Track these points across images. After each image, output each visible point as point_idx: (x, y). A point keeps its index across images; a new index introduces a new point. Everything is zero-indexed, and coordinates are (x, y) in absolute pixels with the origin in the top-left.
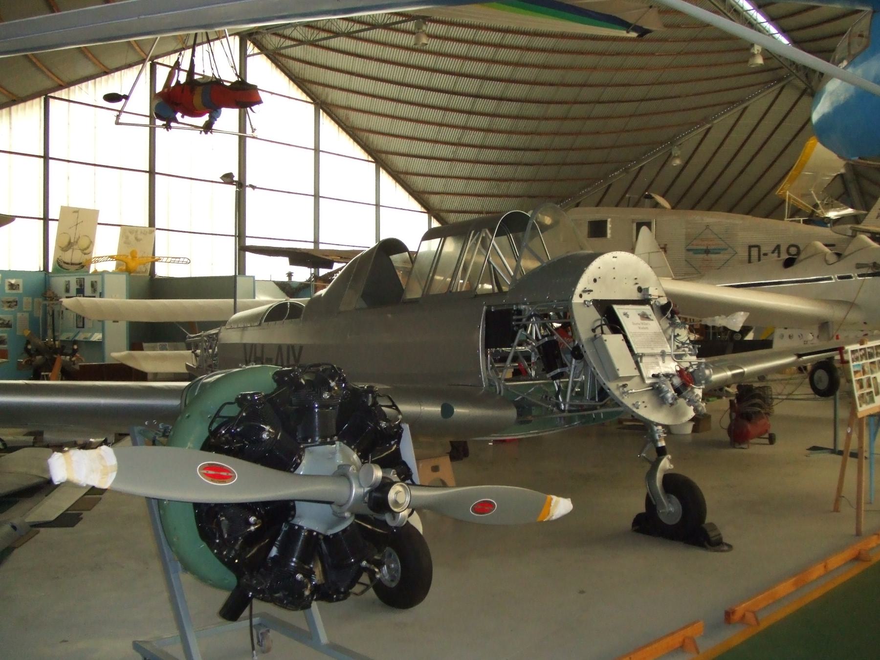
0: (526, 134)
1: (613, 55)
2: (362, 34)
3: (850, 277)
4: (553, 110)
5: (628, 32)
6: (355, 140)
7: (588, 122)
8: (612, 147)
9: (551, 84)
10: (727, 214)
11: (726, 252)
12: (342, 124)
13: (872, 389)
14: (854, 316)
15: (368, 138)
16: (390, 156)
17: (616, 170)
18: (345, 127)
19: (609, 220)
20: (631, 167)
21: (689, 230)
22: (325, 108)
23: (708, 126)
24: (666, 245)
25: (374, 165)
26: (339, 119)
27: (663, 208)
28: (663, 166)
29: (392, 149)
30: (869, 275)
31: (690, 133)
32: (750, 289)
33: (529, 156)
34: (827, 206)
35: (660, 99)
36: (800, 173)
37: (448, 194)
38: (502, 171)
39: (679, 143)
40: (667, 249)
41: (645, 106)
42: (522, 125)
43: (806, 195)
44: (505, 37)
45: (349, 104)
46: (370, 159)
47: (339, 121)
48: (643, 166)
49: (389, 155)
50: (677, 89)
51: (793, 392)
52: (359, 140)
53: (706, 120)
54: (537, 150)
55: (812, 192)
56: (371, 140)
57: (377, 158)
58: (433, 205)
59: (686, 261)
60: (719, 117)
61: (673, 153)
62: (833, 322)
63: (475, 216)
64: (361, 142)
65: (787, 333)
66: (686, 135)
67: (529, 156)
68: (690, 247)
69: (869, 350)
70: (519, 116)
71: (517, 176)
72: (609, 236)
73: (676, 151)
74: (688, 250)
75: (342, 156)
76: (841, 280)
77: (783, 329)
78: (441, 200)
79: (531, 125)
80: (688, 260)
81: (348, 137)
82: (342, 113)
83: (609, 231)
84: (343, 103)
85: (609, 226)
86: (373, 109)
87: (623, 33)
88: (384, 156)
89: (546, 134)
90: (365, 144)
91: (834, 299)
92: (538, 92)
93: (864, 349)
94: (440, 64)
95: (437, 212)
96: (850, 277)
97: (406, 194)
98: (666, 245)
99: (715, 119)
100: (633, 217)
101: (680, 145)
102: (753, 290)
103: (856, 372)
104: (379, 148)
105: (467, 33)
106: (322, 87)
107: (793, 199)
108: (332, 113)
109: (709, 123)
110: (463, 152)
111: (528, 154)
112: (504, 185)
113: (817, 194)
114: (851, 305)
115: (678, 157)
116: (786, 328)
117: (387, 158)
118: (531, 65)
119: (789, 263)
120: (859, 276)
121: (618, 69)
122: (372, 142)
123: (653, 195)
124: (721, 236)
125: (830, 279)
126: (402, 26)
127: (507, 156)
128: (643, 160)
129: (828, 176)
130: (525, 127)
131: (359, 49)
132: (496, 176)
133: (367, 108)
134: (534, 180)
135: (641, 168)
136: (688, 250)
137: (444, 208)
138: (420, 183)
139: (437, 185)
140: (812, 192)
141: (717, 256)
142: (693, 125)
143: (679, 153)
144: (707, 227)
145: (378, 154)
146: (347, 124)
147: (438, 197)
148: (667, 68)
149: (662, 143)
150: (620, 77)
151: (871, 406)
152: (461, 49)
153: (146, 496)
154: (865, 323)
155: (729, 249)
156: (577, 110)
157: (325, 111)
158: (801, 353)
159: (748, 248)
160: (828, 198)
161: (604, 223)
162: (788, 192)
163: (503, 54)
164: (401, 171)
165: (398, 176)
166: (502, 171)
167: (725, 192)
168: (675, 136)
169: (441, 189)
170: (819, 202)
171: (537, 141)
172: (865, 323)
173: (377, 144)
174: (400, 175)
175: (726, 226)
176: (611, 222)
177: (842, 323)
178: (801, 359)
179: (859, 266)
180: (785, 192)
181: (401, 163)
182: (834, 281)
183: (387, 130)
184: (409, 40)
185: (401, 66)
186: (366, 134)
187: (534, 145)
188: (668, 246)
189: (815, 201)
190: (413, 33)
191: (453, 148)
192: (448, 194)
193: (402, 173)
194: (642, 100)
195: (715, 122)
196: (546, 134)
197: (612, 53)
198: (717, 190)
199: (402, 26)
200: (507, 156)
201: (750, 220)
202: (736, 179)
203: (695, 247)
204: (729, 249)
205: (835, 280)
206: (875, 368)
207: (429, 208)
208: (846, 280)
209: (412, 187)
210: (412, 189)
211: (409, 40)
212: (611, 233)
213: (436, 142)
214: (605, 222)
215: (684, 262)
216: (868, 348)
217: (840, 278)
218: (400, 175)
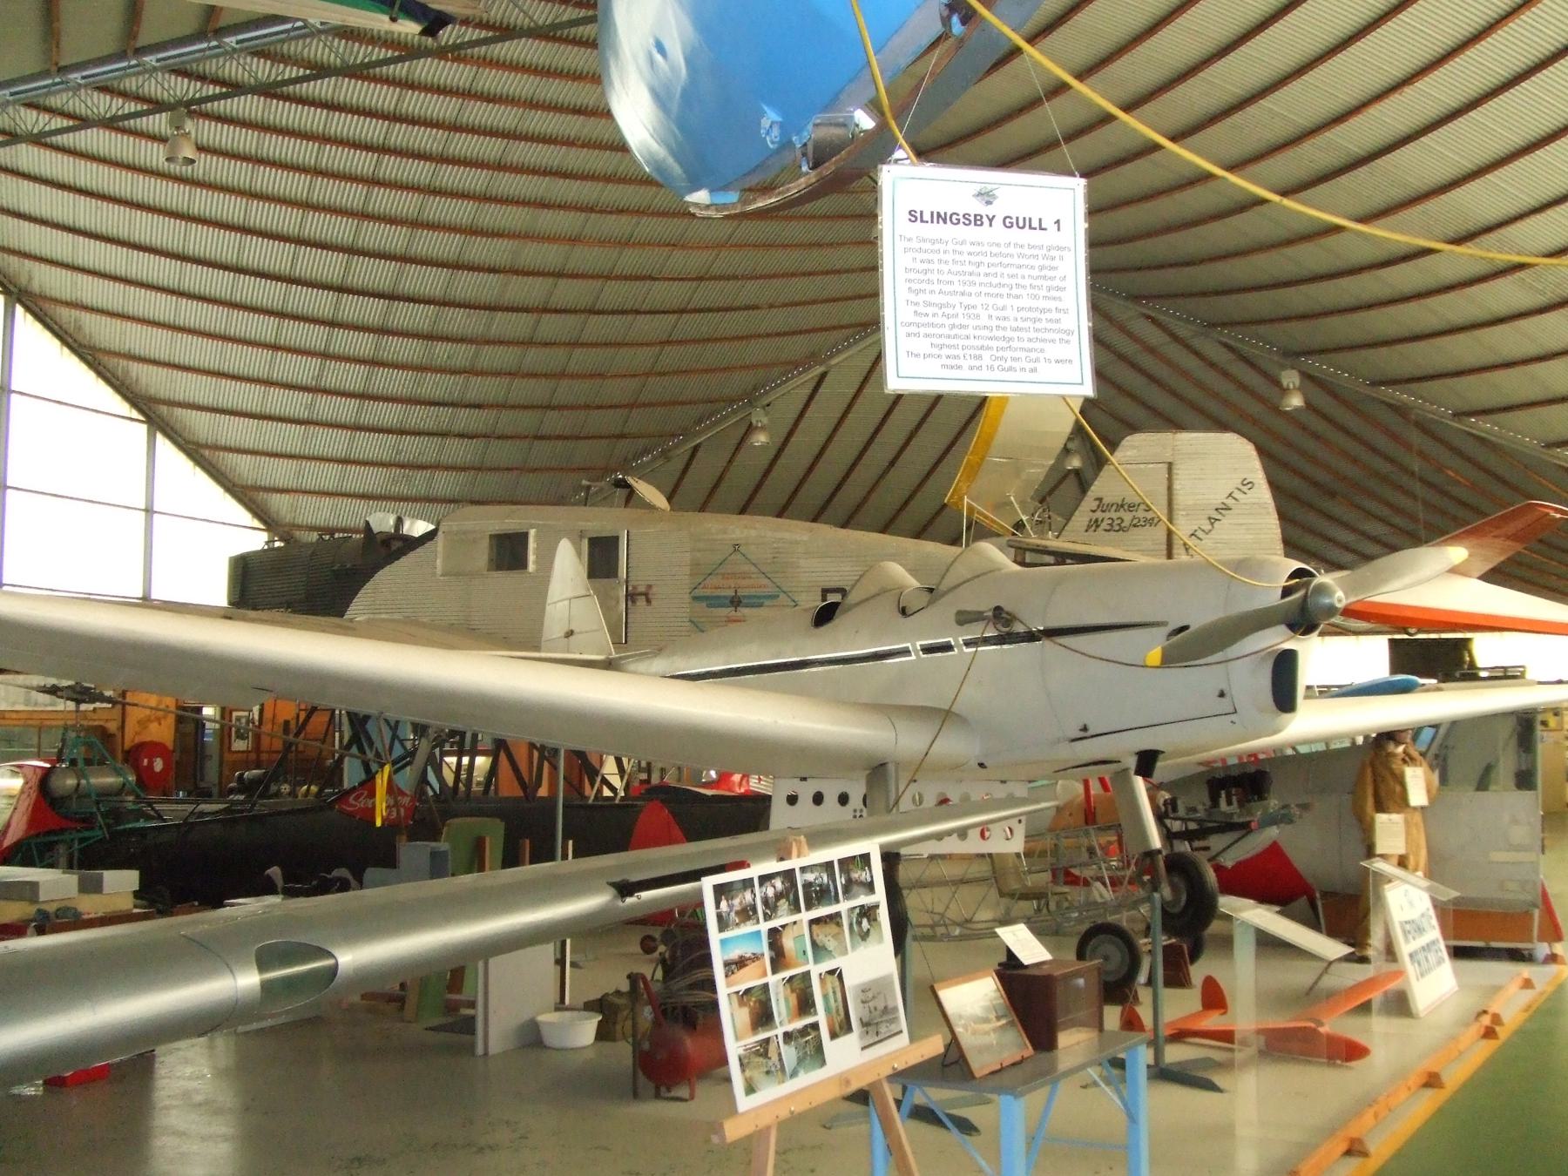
0: (454, 372)
1: (611, 213)
2: (59, 140)
3: (947, 647)
4: (503, 324)
5: (393, 20)
6: (100, 374)
7: (578, 353)
8: (631, 406)
9: (492, 270)
10: (808, 524)
11: (775, 602)
12: (70, 340)
13: (821, 1017)
14: (953, 745)
15: (128, 372)
16: (178, 411)
17: (646, 451)
18: (75, 345)
19: (532, 532)
20: (676, 446)
21: (699, 555)
22: (28, 303)
23: (819, 370)
24: (650, 587)
25: (144, 427)
26: (61, 327)
27: (650, 507)
28: (738, 449)
29: (180, 396)
30: (986, 641)
31: (785, 382)
32: (723, 683)
33: (465, 419)
34: (1040, 526)
35: (719, 310)
36: (982, 459)
37: (305, 492)
38: (412, 448)
39: (766, 402)
40: (650, 596)
41: (691, 325)
42: (442, 352)
43: (1002, 505)
44: (382, 162)
45: (79, 296)
46: (135, 414)
47: (61, 333)
48: (700, 443)
49: (175, 409)
50: (750, 292)
51: (921, 911)
52: (108, 375)
53: (812, 358)
54: (479, 406)
55: (1012, 498)
56: (134, 374)
57: (153, 415)
58: (278, 514)
59: (691, 621)
60: (839, 352)
61: (754, 422)
62: (897, 764)
63: (1210, 659)
64: (113, 380)
65: (806, 791)
66: (778, 386)
67: (465, 419)
68: (699, 592)
69: (810, 877)
70: (434, 333)
71: (445, 459)
72: (531, 567)
73: (759, 417)
74: (696, 598)
75: (115, 415)
76: (930, 655)
77: (797, 781)
78: (292, 506)
79: (461, 354)
80: (695, 620)
81: (83, 367)
82: (65, 315)
83: (531, 558)
84: (66, 295)
85: (532, 545)
86: (130, 309)
87: (383, 21)
88: (164, 409)
89: (497, 374)
90: (123, 384)
91: (912, 703)
92: (468, 285)
93: (789, 875)
94: (256, 217)
95: (286, 529)
96: (947, 647)
97: (218, 490)
98: (650, 587)
99: (831, 357)
100: (582, 525)
101: (768, 405)
102: (729, 684)
103: (736, 965)
104: (152, 391)
105: (306, 151)
106: (16, 258)
107: (978, 513)
108: (46, 315)
109: (821, 365)
110: (328, 407)
111: (464, 413)
112: (420, 476)
113: (1022, 503)
114: (944, 716)
115: (763, 428)
116: (804, 779)
117: (172, 416)
118: (444, 227)
119: (825, 616)
120: (968, 644)
121: (625, 243)
122: (137, 380)
123: (630, 480)
124: (763, 570)
125: (906, 652)
126: (142, 123)
127: (418, 416)
128: (699, 433)
129: (1035, 466)
130: (448, 357)
131: (83, 178)
132: (402, 458)
133: (117, 306)
134: (479, 469)
135: (696, 449)
136: (696, 598)
137: (299, 521)
138: (245, 467)
139: (280, 473)
140: (1012, 498)
141: (754, 610)
142: (797, 365)
143: (765, 420)
144: (736, 547)
145: (152, 405)
146: (80, 338)
147: (286, 498)
148: (722, 246)
149: (732, 401)
150: (631, 260)
151: (809, 1078)
152: (296, 185)
153: (624, 918)
154: (981, 765)
155: (782, 596)
156: (551, 326)
157: (28, 309)
158: (635, 877)
159: (820, 593)
160: (1041, 510)
161: (522, 538)
162: (969, 498)
163: (383, 200)
164: (204, 442)
165: (198, 452)
166: (412, 448)
167: (865, 499)
168: (755, 389)
169: (291, 483)
170: (1024, 518)
171: (479, 388)
172: (981, 765)
173: (147, 385)
174: (202, 451)
175: (775, 545)
176: (537, 536)
177: (920, 767)
178: (630, 900)
179: (965, 618)
180: (962, 500)
181: (201, 425)
182: (913, 657)
183: (164, 355)
184: (154, 155)
185: (220, 229)
186: (123, 363)
187: (471, 396)
188: (654, 589)
189: (1018, 515)
190: (162, 139)
191: (307, 397)
192: (305, 492)
193: (207, 446)
194: (682, 311)
195: (834, 362)
196: (497, 374)
197: (609, 209)
198: (853, 491)
199: (142, 123)
200: (418, 416)
201: (827, 533)
202: (882, 477)
203: (708, 592)
204: (782, 596)
205: (917, 655)
206: (838, 936)
207: (269, 521)
208: (940, 654)
209: (231, 477)
210: (230, 481)
211: (154, 155)
212: (536, 562)
213: (268, 383)
214: (525, 536)
215: (689, 624)
216: (803, 869)
217: (928, 650)
218: (202, 451)
